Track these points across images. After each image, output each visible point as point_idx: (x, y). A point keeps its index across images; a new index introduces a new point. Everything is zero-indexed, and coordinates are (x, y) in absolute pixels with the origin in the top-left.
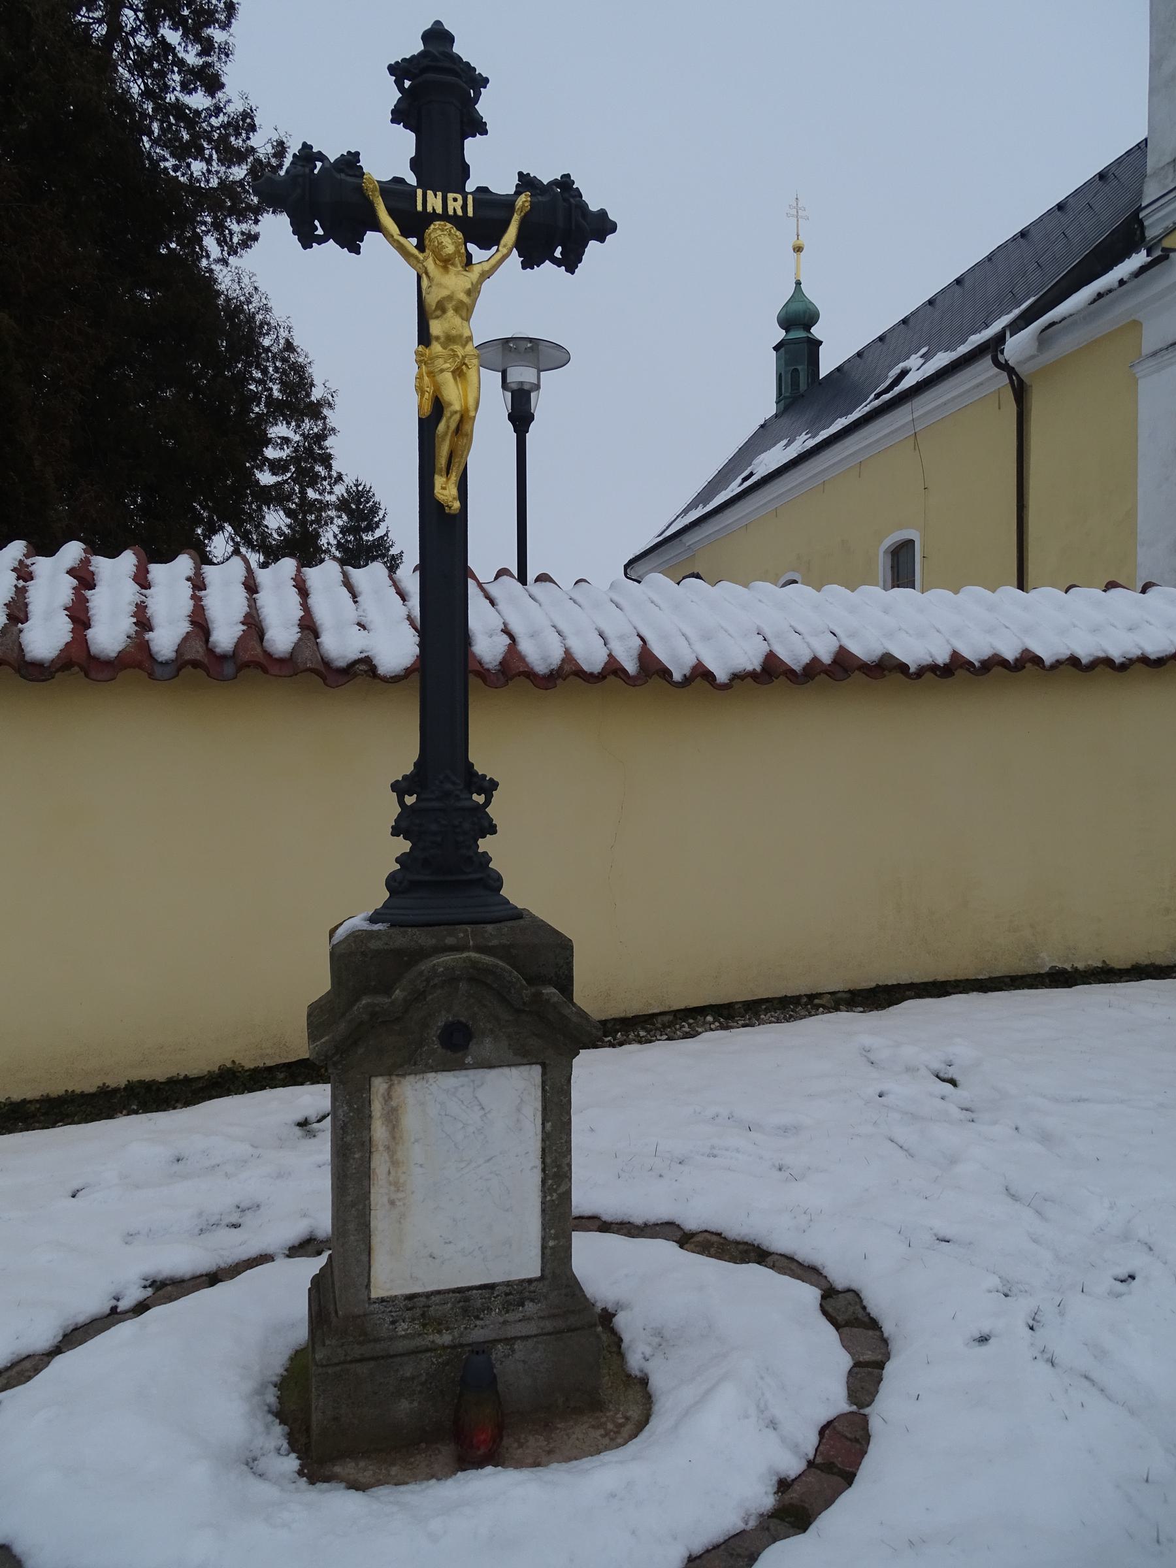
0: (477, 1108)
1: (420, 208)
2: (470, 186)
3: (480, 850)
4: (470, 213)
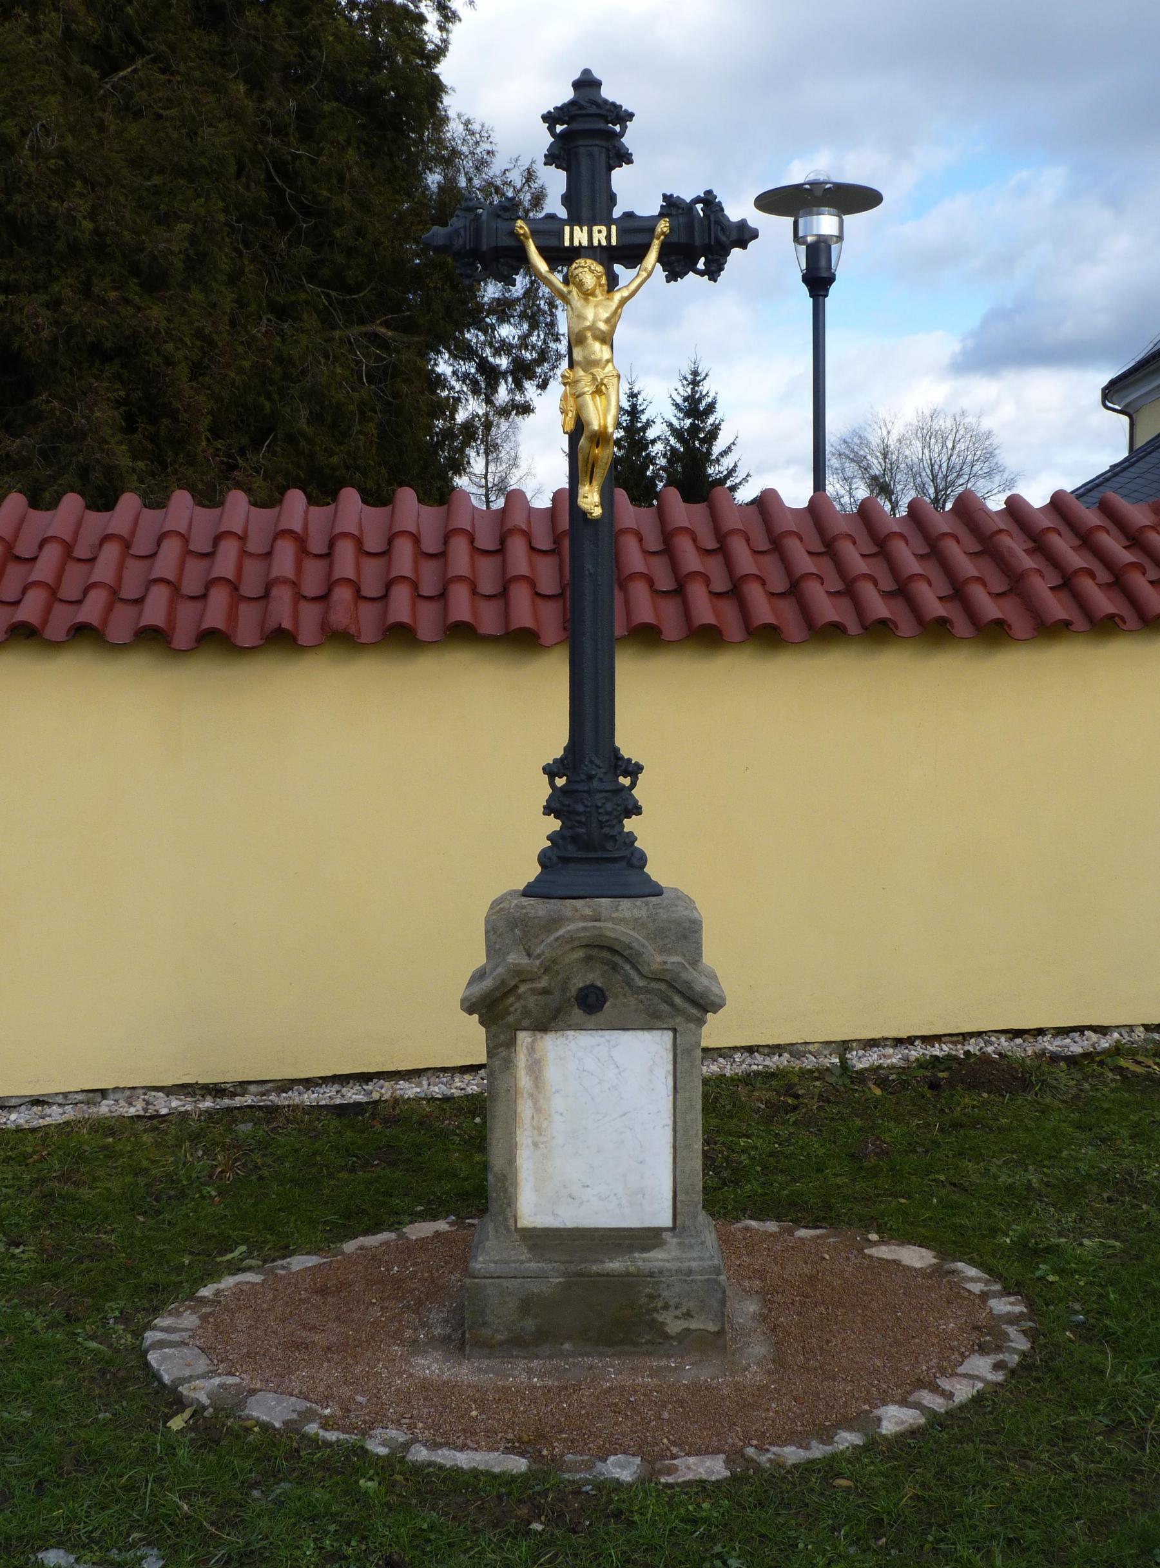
0: (613, 1066)
1: (567, 244)
2: (617, 213)
3: (626, 830)
4: (614, 242)
